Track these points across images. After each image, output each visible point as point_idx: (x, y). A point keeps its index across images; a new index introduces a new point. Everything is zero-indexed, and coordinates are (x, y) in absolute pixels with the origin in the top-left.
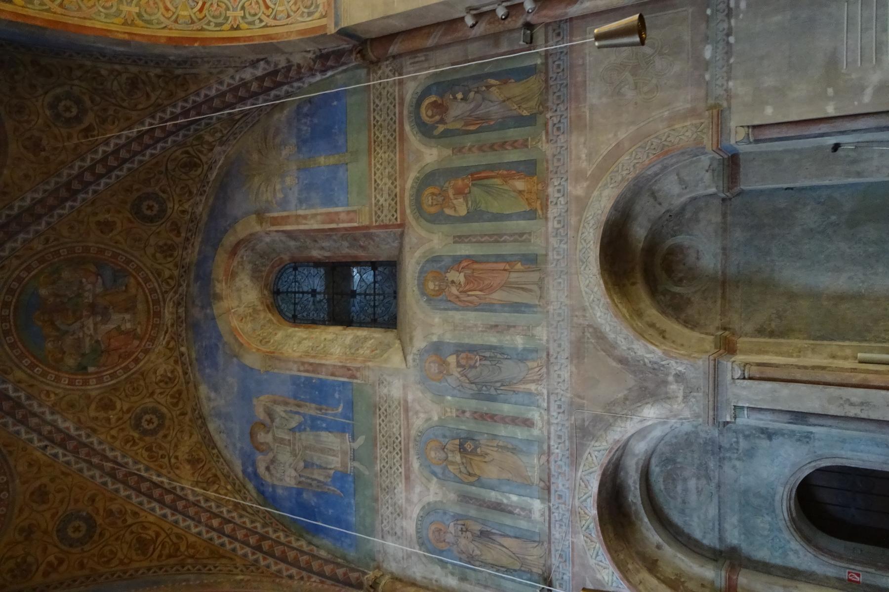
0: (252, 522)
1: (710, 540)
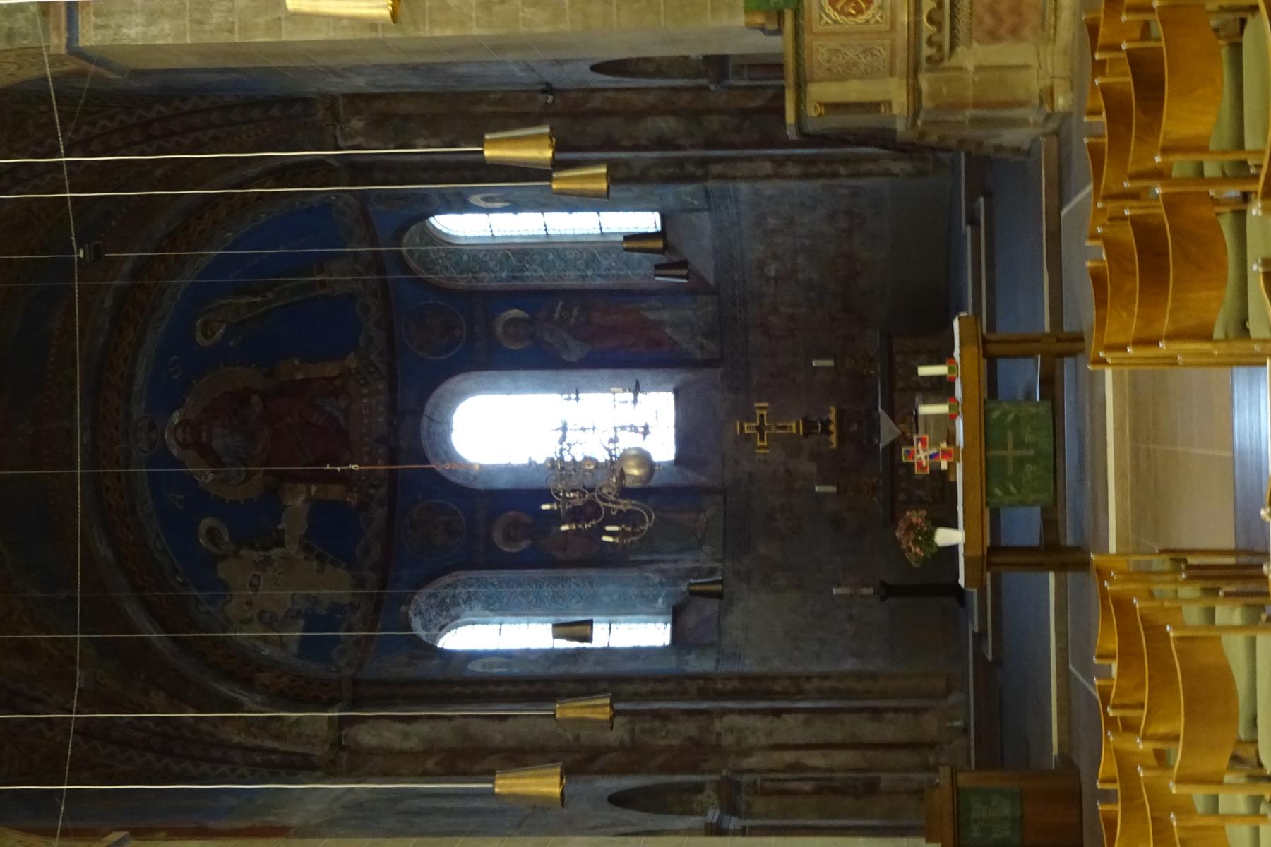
0: (112, 118)
1: (787, 717)
